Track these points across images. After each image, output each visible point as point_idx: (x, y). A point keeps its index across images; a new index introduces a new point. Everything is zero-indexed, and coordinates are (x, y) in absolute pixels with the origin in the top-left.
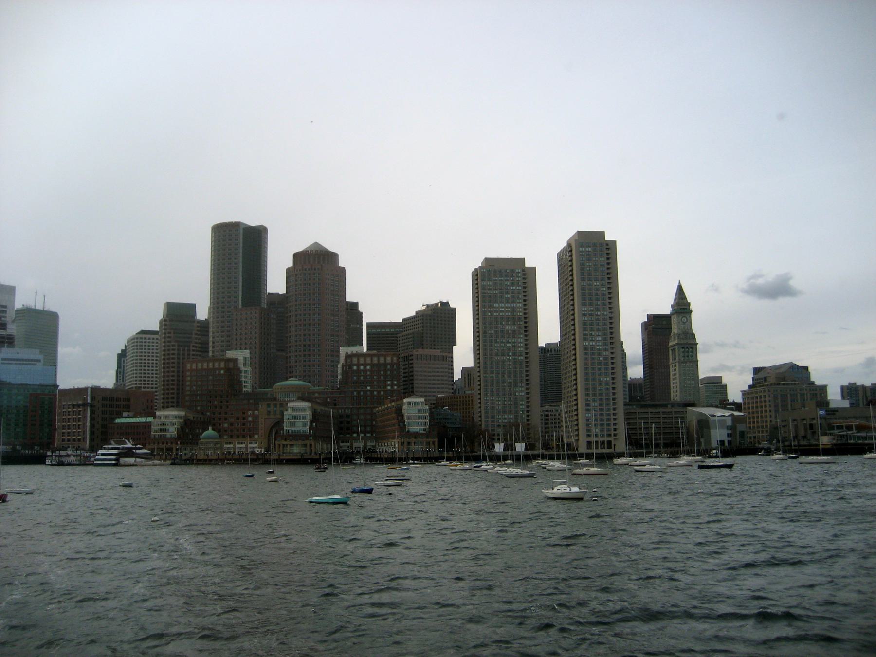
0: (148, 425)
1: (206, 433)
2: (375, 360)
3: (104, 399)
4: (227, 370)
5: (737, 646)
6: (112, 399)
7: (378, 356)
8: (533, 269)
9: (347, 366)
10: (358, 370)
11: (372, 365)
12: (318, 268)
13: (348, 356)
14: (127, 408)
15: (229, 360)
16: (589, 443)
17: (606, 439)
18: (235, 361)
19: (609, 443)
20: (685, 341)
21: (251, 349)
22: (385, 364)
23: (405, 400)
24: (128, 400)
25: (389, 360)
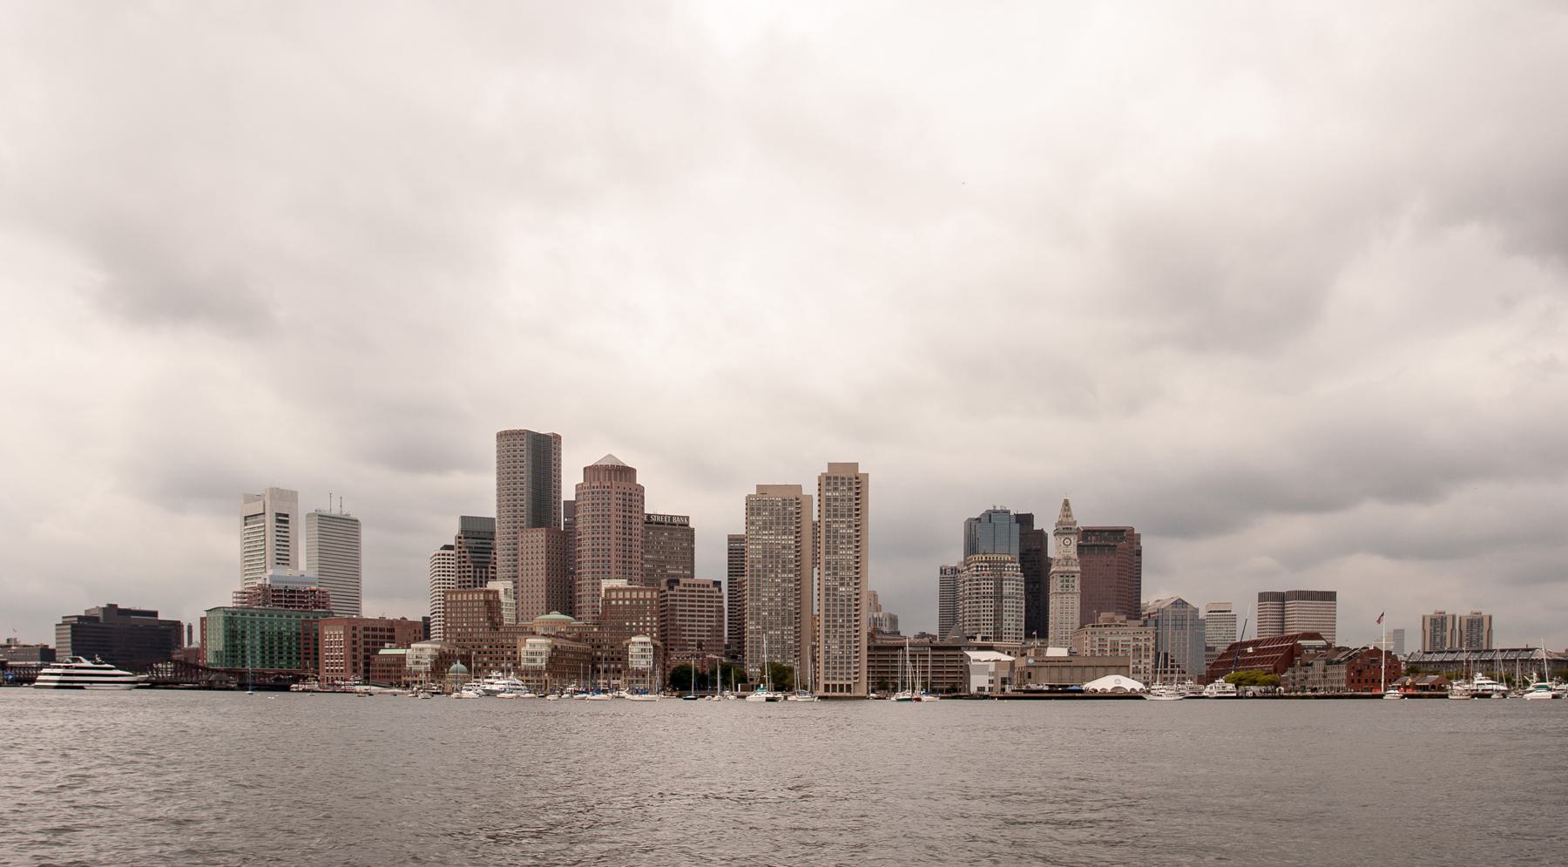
0: (403, 658)
1: (454, 667)
2: (634, 595)
3: (366, 629)
4: (487, 602)
5: (126, 720)
6: (374, 630)
7: (638, 590)
8: (758, 487)
9: (607, 601)
10: (617, 606)
11: (631, 600)
12: (615, 480)
13: (607, 590)
14: (391, 639)
15: (488, 592)
16: (827, 686)
17: (845, 682)
18: (497, 592)
19: (849, 686)
21: (1449, 678)
22: (645, 600)
23: (634, 639)
24: (392, 630)
25: (648, 595)
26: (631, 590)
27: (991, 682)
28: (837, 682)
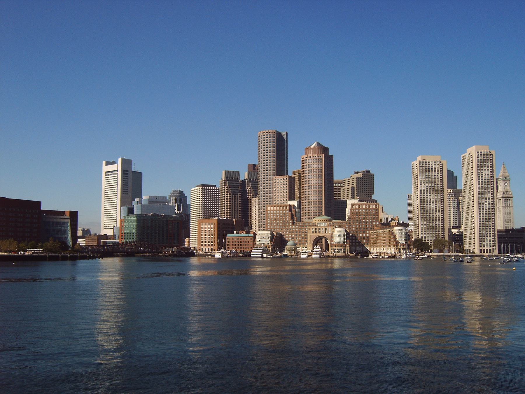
3: (223, 224)
4: (290, 210)
13: (353, 205)
20: (506, 196)
26: (360, 205)
28: (485, 248)
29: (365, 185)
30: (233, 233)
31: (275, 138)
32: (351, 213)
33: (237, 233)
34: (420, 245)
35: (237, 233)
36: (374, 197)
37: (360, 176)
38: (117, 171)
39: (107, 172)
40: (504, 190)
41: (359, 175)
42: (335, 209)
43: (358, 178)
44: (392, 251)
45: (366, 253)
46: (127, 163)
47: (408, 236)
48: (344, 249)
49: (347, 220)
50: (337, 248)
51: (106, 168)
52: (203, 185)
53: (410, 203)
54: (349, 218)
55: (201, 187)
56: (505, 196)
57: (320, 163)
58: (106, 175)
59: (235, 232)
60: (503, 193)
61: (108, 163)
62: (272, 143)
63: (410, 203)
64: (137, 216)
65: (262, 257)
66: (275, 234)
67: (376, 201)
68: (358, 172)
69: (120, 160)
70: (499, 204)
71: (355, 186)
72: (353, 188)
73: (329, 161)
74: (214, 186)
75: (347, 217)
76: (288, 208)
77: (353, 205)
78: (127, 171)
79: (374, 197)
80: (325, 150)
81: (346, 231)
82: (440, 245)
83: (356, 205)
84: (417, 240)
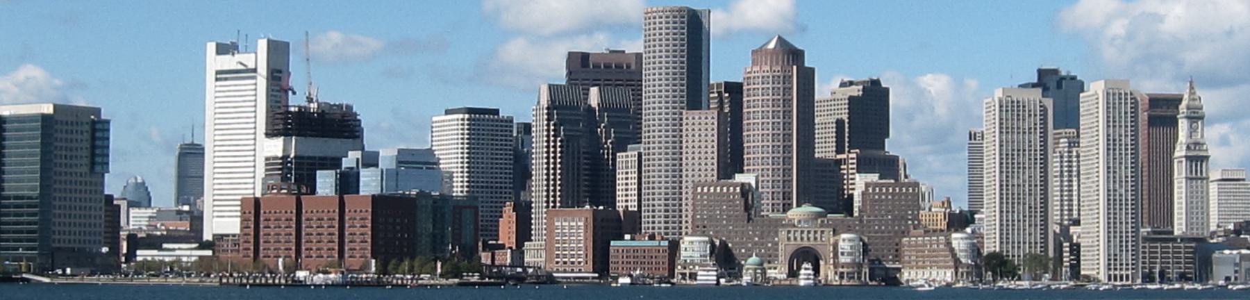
20: (1195, 153)
26: (881, 185)
27: (1236, 272)
29: (870, 110)
30: (622, 238)
31: (685, 25)
32: (863, 200)
33: (633, 239)
34: (999, 265)
35: (633, 239)
36: (891, 147)
37: (856, 94)
38: (255, 70)
39: (218, 72)
40: (1190, 141)
41: (856, 91)
42: (821, 186)
43: (851, 99)
44: (947, 276)
45: (895, 282)
46: (278, 51)
47: (976, 250)
48: (859, 273)
49: (856, 214)
50: (845, 270)
51: (216, 62)
52: (470, 111)
53: (976, 154)
54: (860, 211)
55: (467, 116)
56: (1190, 154)
57: (787, 85)
58: (217, 79)
59: (627, 237)
60: (1188, 148)
61: (222, 49)
62: (671, 25)
63: (976, 154)
64: (375, 199)
65: (718, 283)
66: (718, 243)
67: (894, 161)
68: (851, 83)
69: (262, 45)
70: (1180, 173)
71: (845, 117)
72: (840, 123)
73: (807, 78)
74: (496, 112)
75: (856, 209)
76: (738, 189)
77: (867, 185)
78: (280, 72)
79: (891, 147)
80: (795, 55)
81: (861, 240)
82: (1038, 263)
83: (875, 185)
84: (992, 256)
